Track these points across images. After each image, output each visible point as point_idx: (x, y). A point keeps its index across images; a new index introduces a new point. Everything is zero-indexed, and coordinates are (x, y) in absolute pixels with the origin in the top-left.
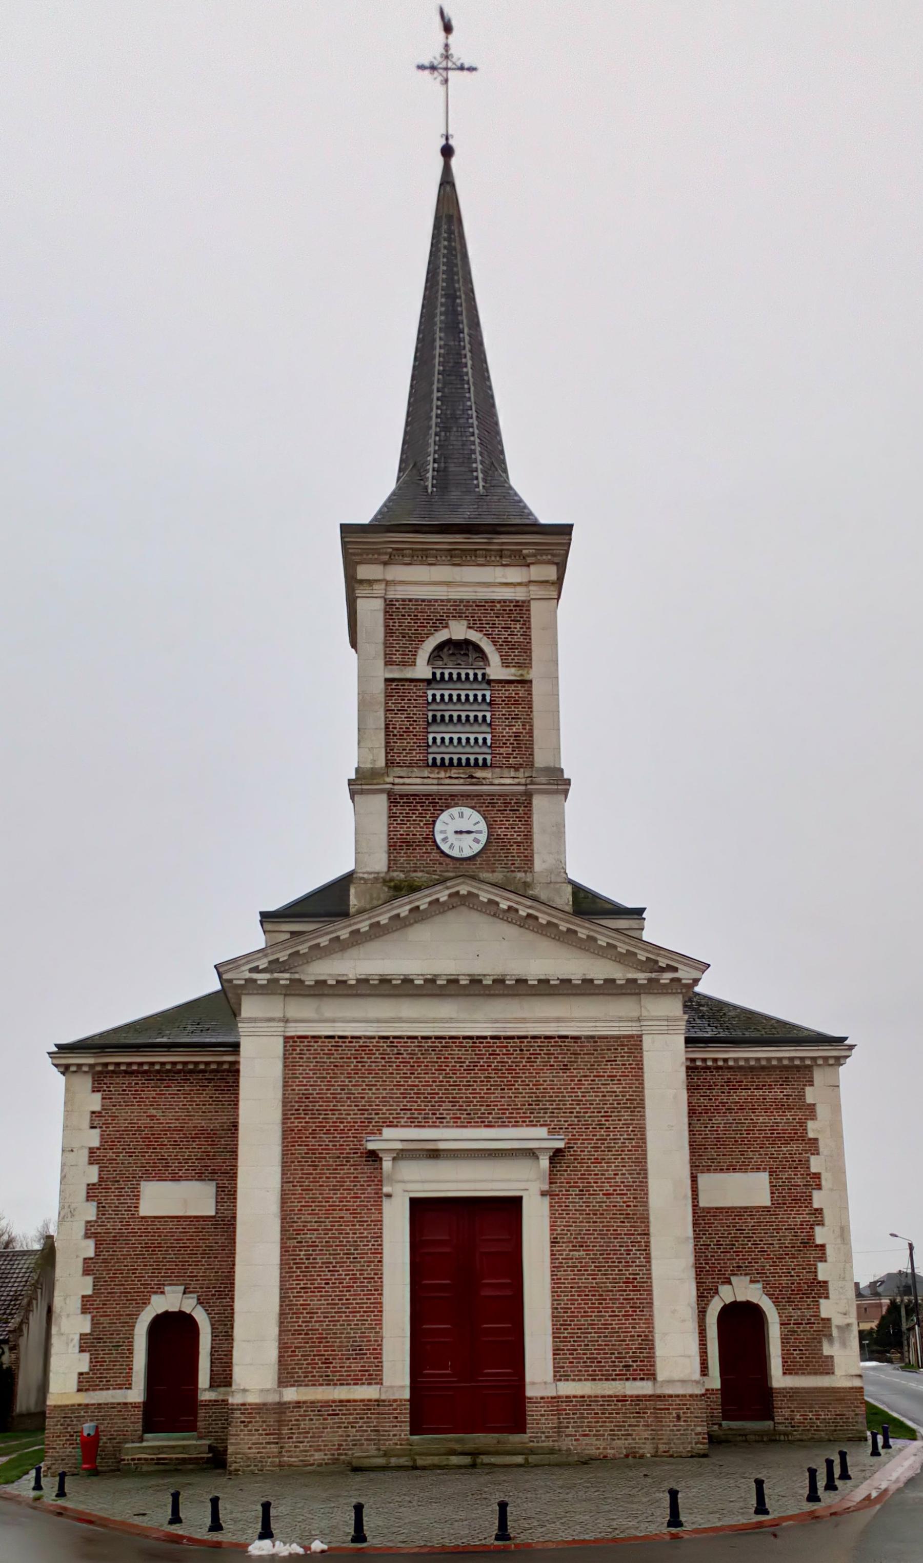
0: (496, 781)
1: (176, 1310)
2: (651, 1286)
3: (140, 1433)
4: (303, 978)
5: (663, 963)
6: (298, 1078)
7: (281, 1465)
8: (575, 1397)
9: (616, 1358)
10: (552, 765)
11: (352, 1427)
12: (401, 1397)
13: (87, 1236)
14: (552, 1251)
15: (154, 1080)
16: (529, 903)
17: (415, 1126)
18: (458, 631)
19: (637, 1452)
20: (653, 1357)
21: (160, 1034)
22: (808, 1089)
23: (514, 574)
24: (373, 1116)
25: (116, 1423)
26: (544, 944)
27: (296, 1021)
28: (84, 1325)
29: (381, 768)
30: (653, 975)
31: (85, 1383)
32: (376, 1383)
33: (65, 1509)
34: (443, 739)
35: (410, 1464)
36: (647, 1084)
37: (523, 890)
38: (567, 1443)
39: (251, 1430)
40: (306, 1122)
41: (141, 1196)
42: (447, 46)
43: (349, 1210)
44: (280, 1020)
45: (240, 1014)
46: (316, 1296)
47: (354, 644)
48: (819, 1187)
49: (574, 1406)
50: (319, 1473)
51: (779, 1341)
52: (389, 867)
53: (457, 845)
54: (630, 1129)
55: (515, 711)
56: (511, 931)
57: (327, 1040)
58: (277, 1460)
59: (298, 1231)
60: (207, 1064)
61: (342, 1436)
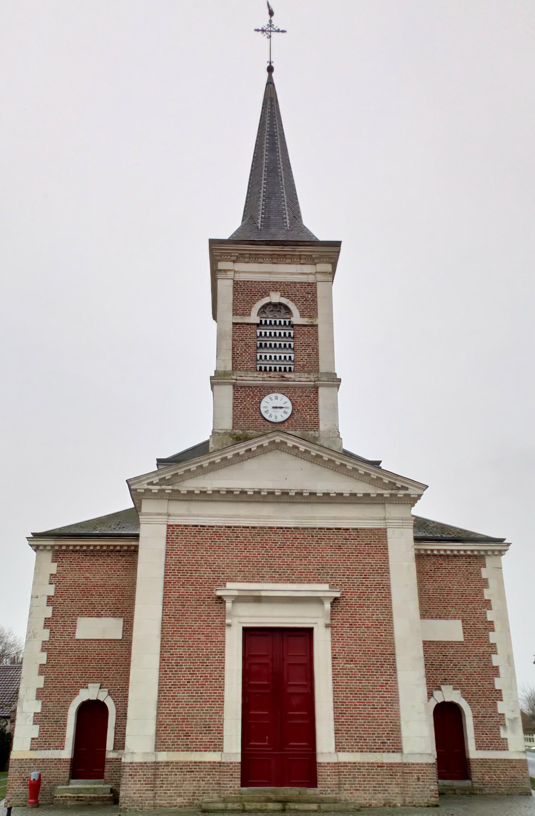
0: (297, 380)
1: (95, 699)
2: (397, 689)
3: (67, 779)
4: (180, 489)
5: (399, 484)
6: (174, 550)
8: (349, 763)
9: (376, 737)
10: (330, 371)
11: (203, 780)
12: (235, 761)
13: (43, 650)
14: (333, 663)
15: (89, 557)
16: (317, 447)
17: (246, 582)
18: (275, 298)
19: (392, 803)
20: (400, 737)
21: (95, 529)
22: (483, 570)
24: (221, 575)
25: (53, 772)
26: (328, 474)
27: (175, 516)
29: (230, 371)
30: (393, 492)
32: (219, 751)
34: (266, 356)
35: (241, 808)
36: (391, 559)
37: (314, 441)
38: (344, 795)
39: (136, 781)
40: (179, 578)
41: (77, 627)
42: (271, 21)
43: (204, 634)
44: (165, 515)
45: (140, 511)
46: (182, 690)
47: (215, 317)
48: (493, 630)
49: (349, 769)
51: (473, 728)
52: (233, 427)
53: (274, 414)
54: (381, 586)
56: (306, 465)
57: (193, 528)
58: (152, 802)
59: (171, 648)
60: (122, 546)
61: (196, 787)
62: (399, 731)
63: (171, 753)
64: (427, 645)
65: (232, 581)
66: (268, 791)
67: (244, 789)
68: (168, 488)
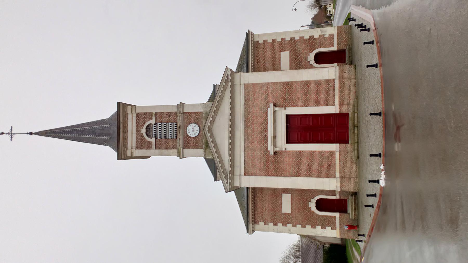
7: (357, 178)
13: (296, 227)
15: (256, 208)
16: (210, 113)
18: (143, 131)
21: (245, 207)
22: (260, 42)
23: (130, 117)
26: (221, 108)
28: (319, 228)
31: (334, 228)
33: (368, 235)
37: (208, 114)
38: (352, 102)
42: (6, 134)
47: (149, 157)
50: (359, 167)
55: (164, 117)
62: (326, 80)
63: (336, 172)
64: (292, 68)
65: (267, 148)
66: (350, 133)
67: (350, 142)
68: (229, 175)
